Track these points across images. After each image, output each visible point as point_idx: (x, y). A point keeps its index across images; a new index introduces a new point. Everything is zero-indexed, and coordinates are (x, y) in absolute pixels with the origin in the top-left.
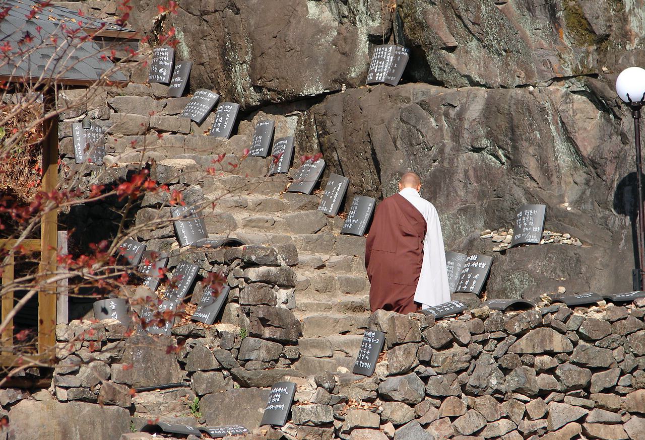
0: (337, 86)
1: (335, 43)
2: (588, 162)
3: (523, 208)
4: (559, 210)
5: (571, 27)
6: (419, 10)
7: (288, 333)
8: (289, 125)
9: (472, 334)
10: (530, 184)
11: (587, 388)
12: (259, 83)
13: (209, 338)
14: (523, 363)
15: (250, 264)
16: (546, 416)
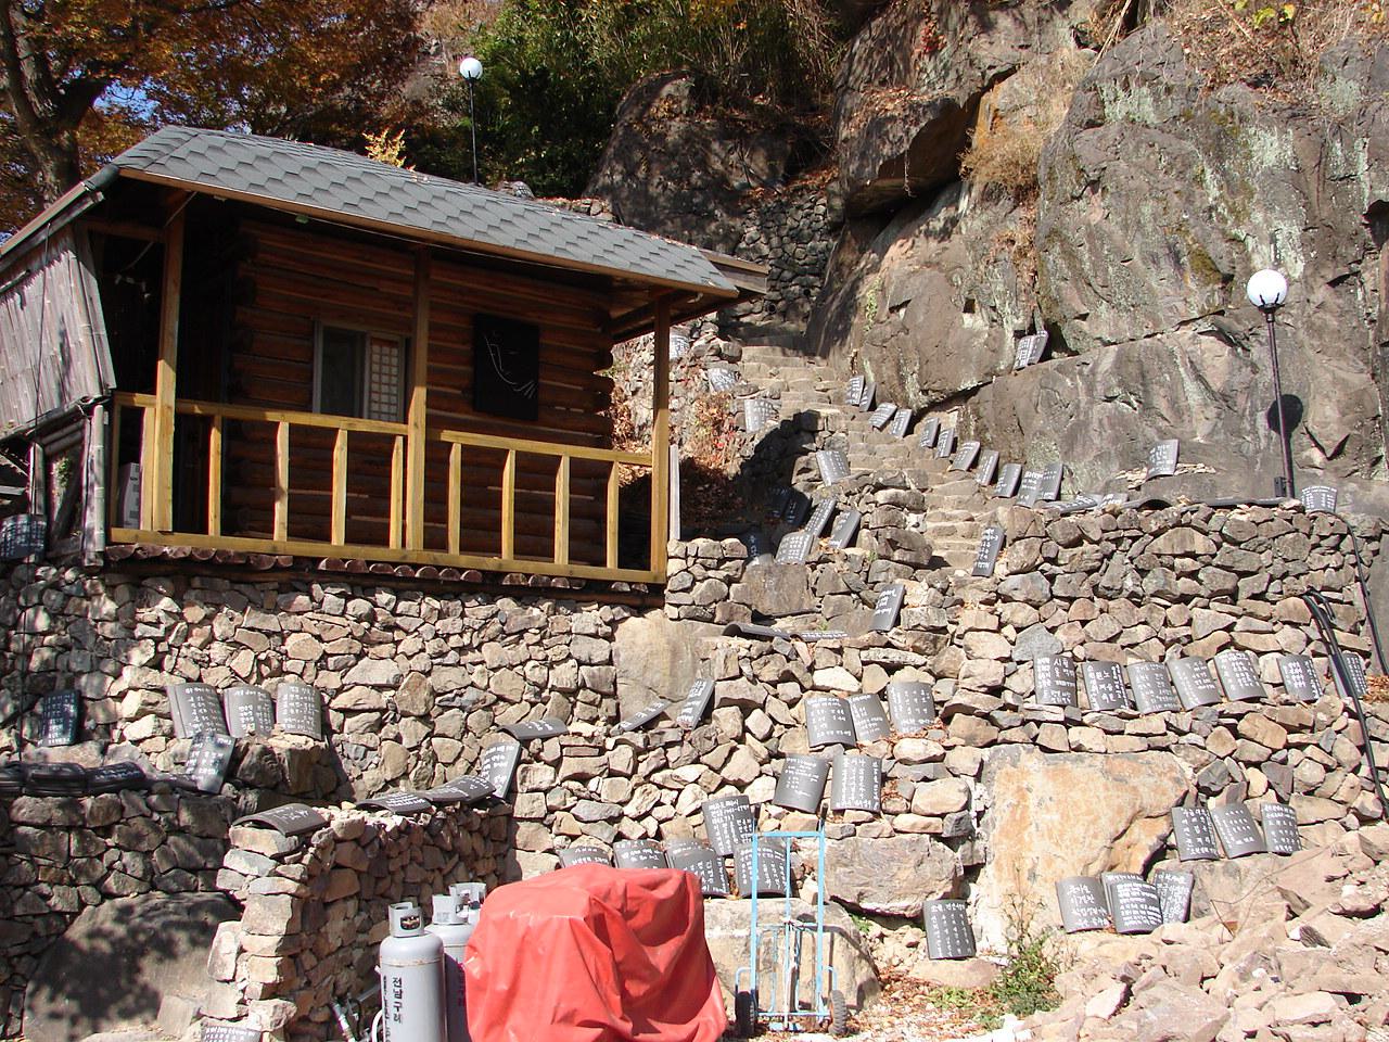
0: (989, 379)
1: (986, 343)
2: (1218, 396)
3: (1156, 445)
4: (1192, 443)
5: (1195, 270)
6: (1053, 288)
7: (918, 556)
8: (950, 419)
9: (1104, 531)
10: (1162, 424)
11: (1233, 596)
12: (925, 387)
13: (839, 562)
14: (1162, 564)
15: (879, 487)
16: (1189, 623)
